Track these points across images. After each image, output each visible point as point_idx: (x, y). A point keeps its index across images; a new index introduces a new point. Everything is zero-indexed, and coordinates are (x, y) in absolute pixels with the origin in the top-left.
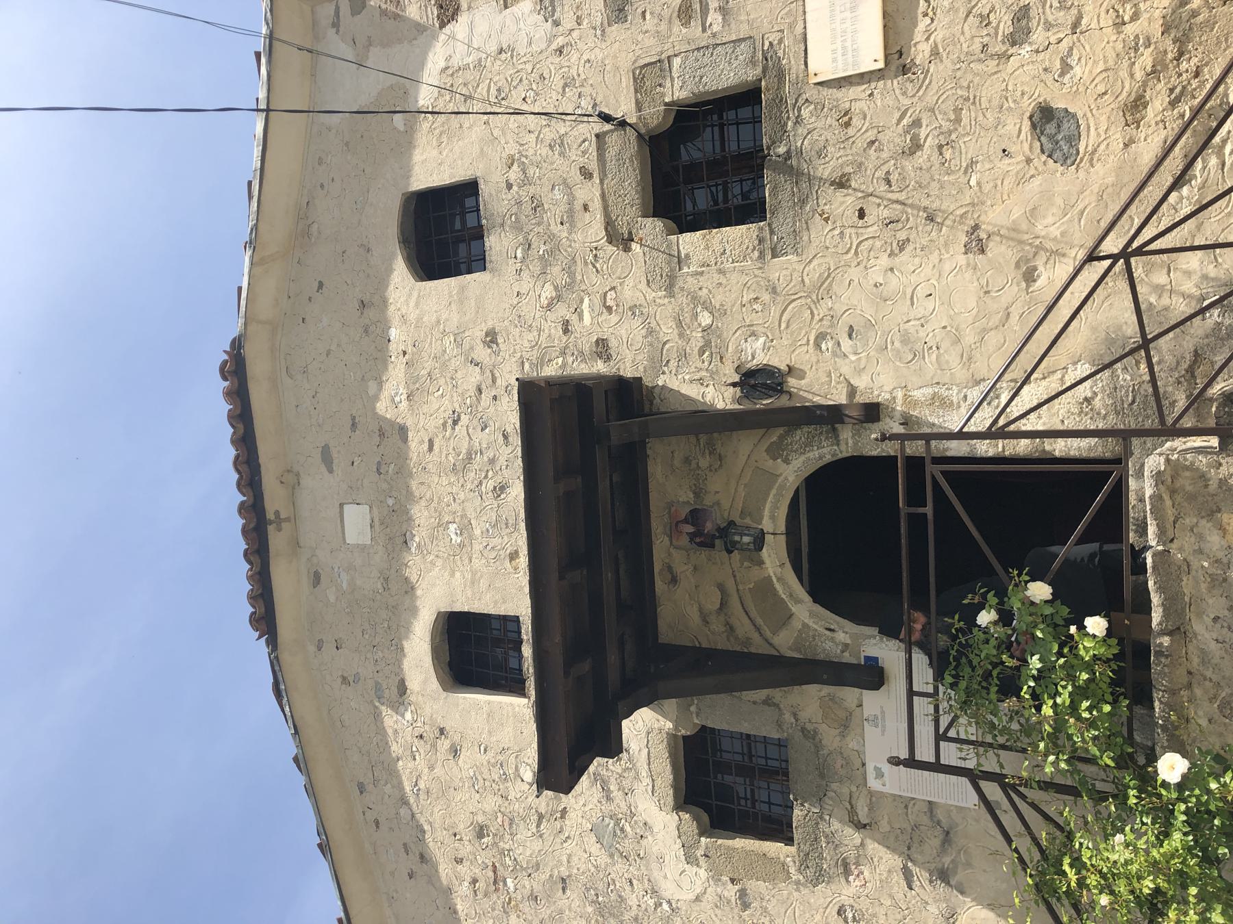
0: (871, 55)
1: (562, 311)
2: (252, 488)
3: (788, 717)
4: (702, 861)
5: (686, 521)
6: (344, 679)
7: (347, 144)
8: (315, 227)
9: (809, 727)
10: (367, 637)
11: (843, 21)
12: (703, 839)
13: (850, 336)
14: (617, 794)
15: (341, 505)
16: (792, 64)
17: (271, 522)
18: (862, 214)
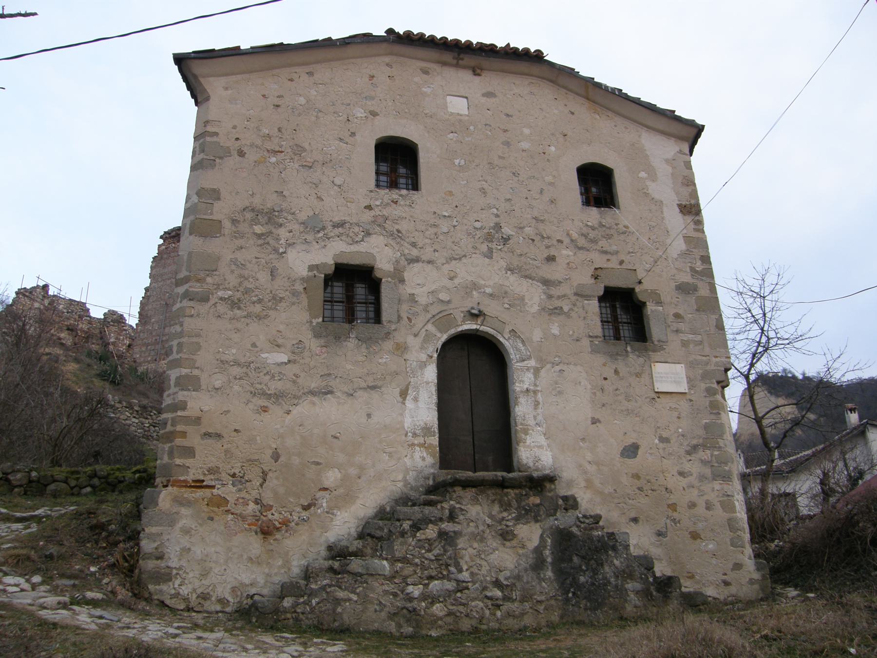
0: (660, 387)
1: (566, 241)
2: (485, 70)
3: (393, 327)
6: (373, 77)
7: (633, 145)
8: (598, 117)
9: (391, 336)
10: (398, 97)
11: (671, 378)
12: (323, 276)
13: (560, 370)
15: (466, 98)
17: (459, 55)
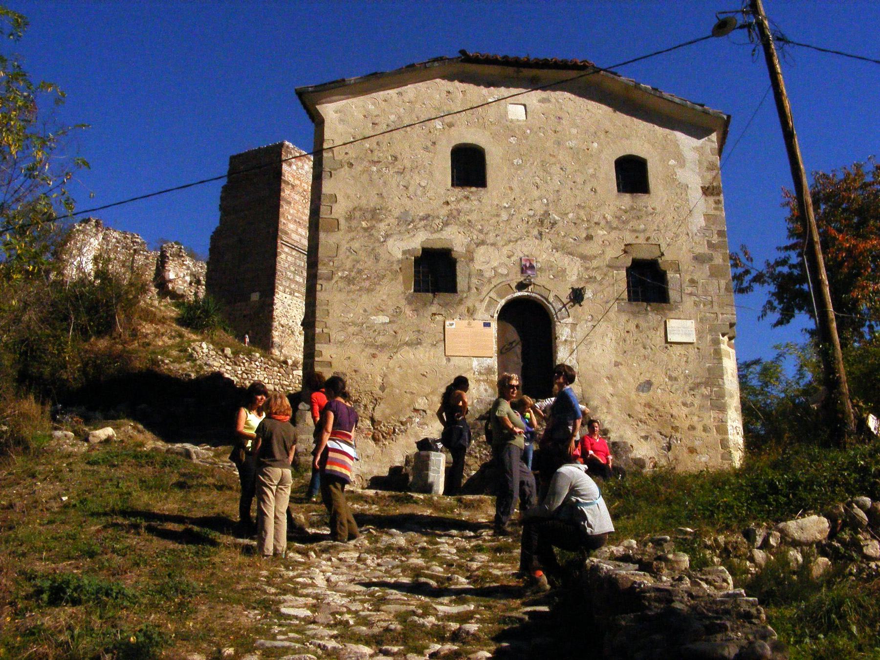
1: (603, 223)
4: (404, 257)
5: (530, 264)
14: (423, 223)
16: (671, 315)
18: (628, 332)
